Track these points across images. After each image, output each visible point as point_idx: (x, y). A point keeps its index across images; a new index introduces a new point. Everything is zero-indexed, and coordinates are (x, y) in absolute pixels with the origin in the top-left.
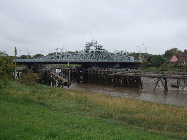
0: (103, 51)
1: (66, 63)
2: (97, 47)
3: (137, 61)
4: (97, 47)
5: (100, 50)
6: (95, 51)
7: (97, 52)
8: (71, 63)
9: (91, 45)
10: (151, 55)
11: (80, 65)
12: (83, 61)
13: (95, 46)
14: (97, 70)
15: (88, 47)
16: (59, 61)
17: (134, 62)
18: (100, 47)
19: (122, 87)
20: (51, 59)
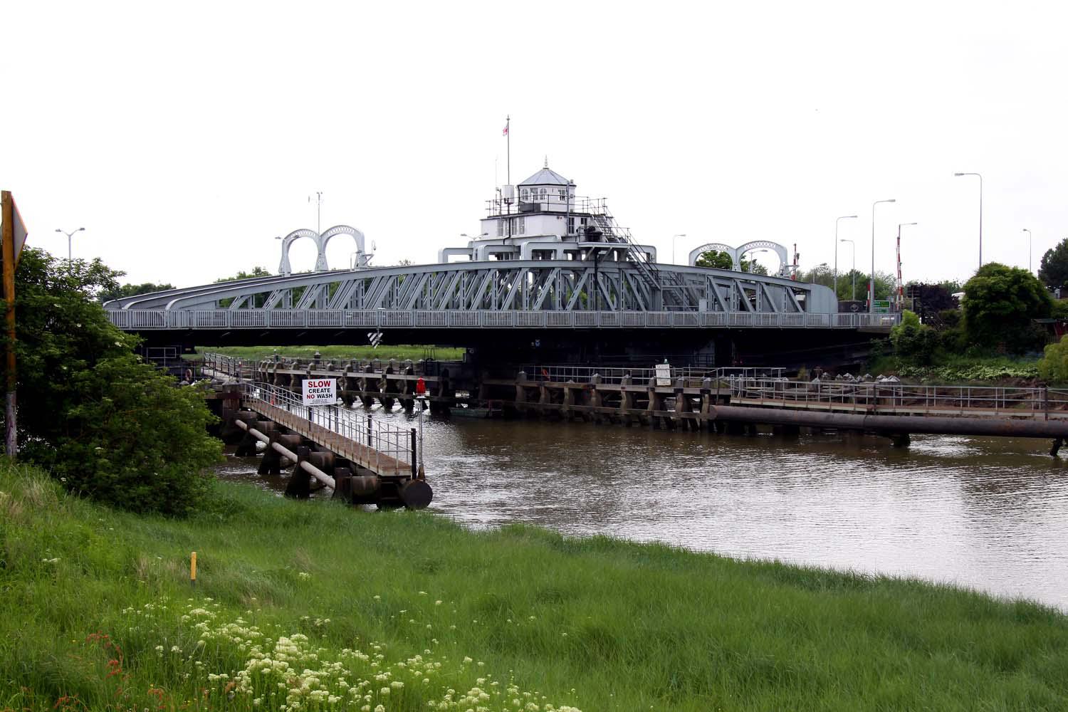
0: (621, 251)
1: (356, 336)
2: (577, 221)
3: (855, 320)
4: (577, 221)
5: (594, 245)
6: (560, 248)
7: (576, 253)
8: (393, 336)
9: (532, 210)
10: (1015, 270)
11: (455, 354)
12: (480, 319)
13: (558, 214)
14: (581, 386)
15: (510, 218)
16: (268, 323)
17: (835, 324)
18: (596, 224)
19: (286, 456)
20: (245, 305)
